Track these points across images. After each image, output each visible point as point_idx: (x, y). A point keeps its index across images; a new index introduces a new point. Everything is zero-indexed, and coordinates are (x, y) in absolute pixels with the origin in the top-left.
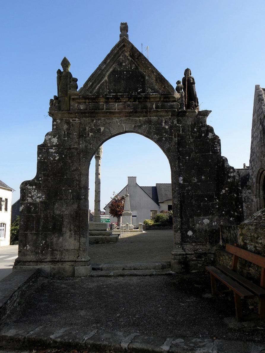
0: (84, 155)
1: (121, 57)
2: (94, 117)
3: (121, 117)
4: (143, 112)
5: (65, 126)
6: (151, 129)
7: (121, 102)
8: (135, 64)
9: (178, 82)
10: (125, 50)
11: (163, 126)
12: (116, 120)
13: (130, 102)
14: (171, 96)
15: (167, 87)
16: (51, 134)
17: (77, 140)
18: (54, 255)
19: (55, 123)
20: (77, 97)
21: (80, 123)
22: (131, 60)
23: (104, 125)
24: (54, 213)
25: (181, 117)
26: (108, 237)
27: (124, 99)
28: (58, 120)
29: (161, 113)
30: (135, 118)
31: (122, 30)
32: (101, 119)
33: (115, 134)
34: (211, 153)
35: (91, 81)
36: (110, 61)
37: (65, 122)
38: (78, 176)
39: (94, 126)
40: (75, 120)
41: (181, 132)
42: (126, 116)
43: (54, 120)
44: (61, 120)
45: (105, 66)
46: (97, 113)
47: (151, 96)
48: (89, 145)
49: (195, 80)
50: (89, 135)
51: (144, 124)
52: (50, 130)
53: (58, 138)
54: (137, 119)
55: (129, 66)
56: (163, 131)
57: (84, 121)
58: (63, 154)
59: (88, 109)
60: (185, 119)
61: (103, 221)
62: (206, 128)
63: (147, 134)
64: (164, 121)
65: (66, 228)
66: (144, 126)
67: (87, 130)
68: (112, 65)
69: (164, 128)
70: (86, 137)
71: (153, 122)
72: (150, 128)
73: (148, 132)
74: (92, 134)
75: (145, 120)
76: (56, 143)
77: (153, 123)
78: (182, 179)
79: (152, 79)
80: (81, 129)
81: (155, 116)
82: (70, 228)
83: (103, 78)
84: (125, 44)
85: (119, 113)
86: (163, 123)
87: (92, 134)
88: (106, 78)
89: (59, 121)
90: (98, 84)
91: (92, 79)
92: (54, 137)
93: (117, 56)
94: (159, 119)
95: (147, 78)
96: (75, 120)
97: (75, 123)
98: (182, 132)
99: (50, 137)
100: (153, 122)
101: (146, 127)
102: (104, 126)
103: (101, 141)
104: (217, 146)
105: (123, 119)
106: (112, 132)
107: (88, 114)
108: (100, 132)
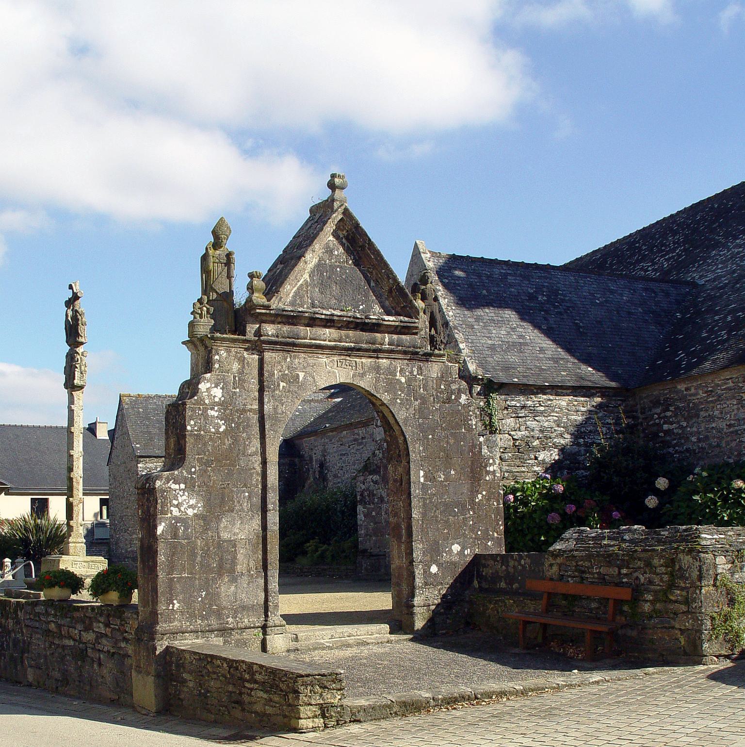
41: (422, 389)
50: (279, 385)
53: (222, 388)
92: (216, 387)
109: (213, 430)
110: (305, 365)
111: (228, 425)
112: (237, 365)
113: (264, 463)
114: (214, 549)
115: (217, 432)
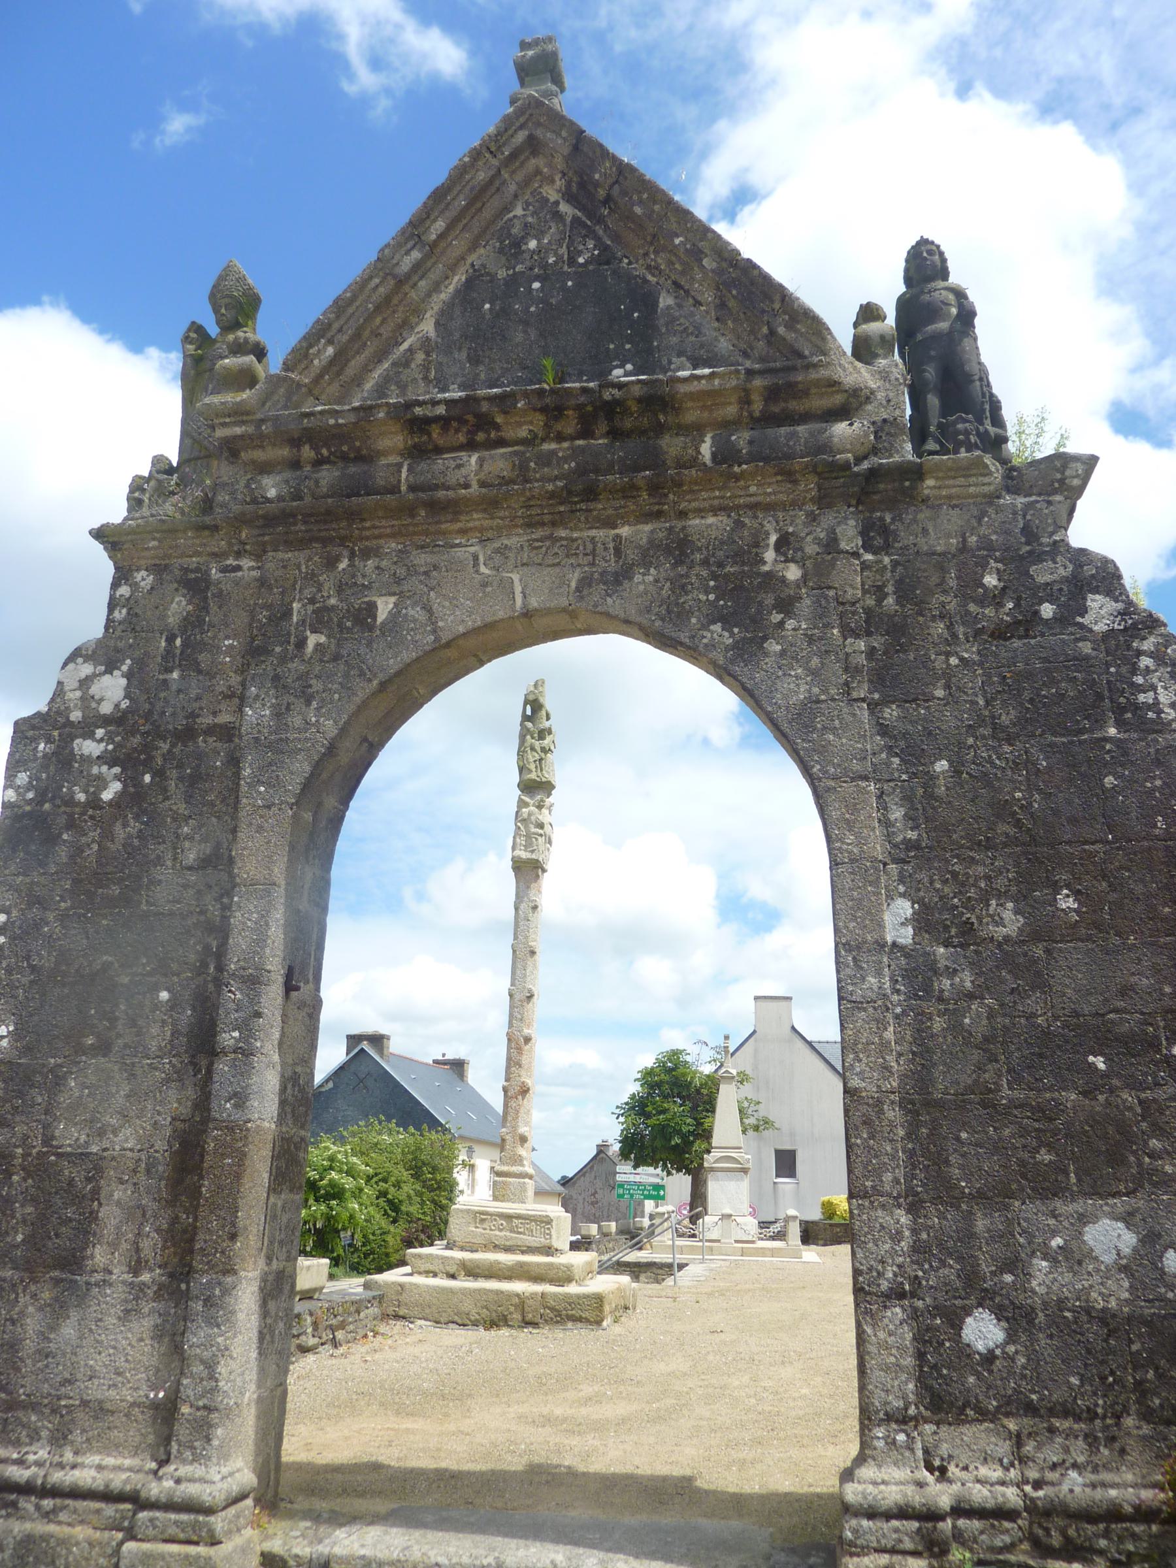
0: (260, 769)
1: (519, 211)
2: (343, 541)
3: (499, 529)
4: (638, 489)
5: (174, 605)
6: (686, 593)
7: (501, 443)
8: (597, 239)
9: (869, 313)
10: (538, 172)
11: (766, 568)
12: (472, 549)
13: (560, 438)
14: (813, 375)
15: (790, 326)
16: (94, 652)
17: (235, 680)
18: (13, 1437)
19: (124, 590)
20: (244, 428)
21: (262, 582)
22: (576, 219)
23: (398, 581)
24: (53, 1138)
25: (890, 510)
26: (555, 1295)
27: (520, 424)
28: (143, 573)
29: (753, 489)
30: (585, 534)
31: (527, 75)
32: (379, 547)
33: (461, 629)
34: (1112, 731)
35: (329, 335)
36: (449, 228)
37: (179, 582)
38: (218, 899)
39: (340, 589)
40: (238, 568)
41: (890, 600)
42: (530, 525)
43: (122, 576)
44: (158, 570)
45: (416, 255)
46: (353, 516)
47: (683, 389)
48: (299, 704)
49: (972, 296)
50: (301, 643)
51: (646, 561)
52: (96, 629)
53: (129, 676)
54: (599, 534)
55: (563, 251)
56: (769, 600)
57: (284, 567)
58: (147, 765)
59: (308, 499)
60: (915, 520)
61: (632, 1196)
62: (1063, 570)
63: (663, 620)
64: (773, 538)
65: (114, 1246)
66: (644, 574)
67: (295, 619)
68: (463, 258)
69: (772, 580)
70: (284, 659)
71: (699, 549)
72: (680, 587)
73: (669, 612)
74: (322, 639)
75: (651, 542)
76: (117, 706)
77: (698, 557)
78: (910, 912)
79: (698, 303)
80: (263, 616)
81: (715, 511)
82: (138, 1250)
83: (406, 326)
84: (539, 133)
85: (490, 505)
86: (768, 545)
87: (322, 639)
88: (428, 327)
89: (145, 579)
90: (380, 361)
91: (336, 326)
92: (109, 671)
93: (494, 204)
94: (739, 524)
95: (665, 301)
96: (238, 568)
97: (237, 583)
98: (898, 602)
99: (87, 669)
100: (699, 549)
101: (656, 581)
102: (396, 589)
103: (370, 680)
104: (1155, 680)
105: (512, 541)
106: (440, 624)
107: (305, 523)
108: (371, 628)
109: (81, 797)
110: (401, 572)
111: (130, 780)
112: (184, 603)
113: (348, 319)
114: (25, 1179)
115: (94, 802)
